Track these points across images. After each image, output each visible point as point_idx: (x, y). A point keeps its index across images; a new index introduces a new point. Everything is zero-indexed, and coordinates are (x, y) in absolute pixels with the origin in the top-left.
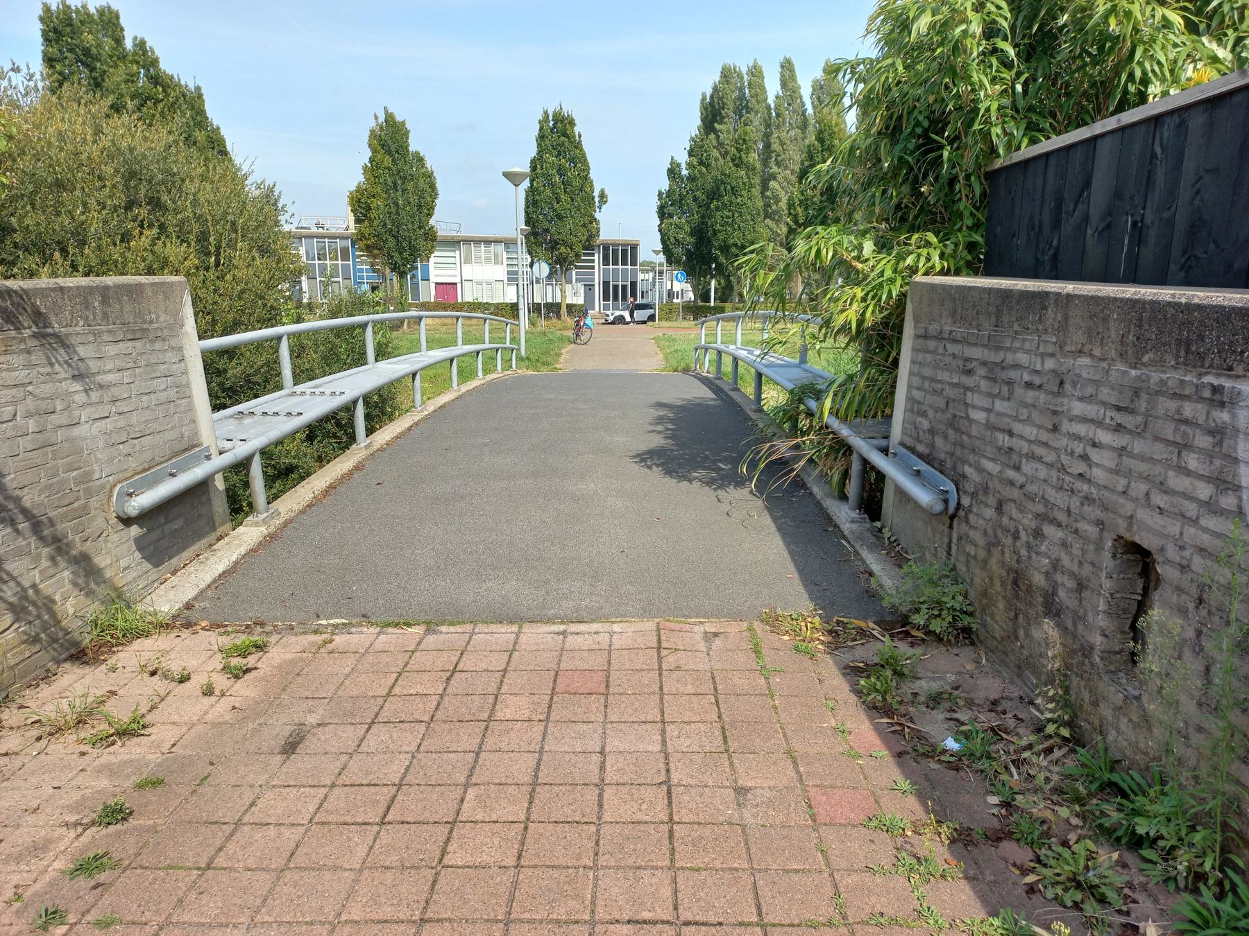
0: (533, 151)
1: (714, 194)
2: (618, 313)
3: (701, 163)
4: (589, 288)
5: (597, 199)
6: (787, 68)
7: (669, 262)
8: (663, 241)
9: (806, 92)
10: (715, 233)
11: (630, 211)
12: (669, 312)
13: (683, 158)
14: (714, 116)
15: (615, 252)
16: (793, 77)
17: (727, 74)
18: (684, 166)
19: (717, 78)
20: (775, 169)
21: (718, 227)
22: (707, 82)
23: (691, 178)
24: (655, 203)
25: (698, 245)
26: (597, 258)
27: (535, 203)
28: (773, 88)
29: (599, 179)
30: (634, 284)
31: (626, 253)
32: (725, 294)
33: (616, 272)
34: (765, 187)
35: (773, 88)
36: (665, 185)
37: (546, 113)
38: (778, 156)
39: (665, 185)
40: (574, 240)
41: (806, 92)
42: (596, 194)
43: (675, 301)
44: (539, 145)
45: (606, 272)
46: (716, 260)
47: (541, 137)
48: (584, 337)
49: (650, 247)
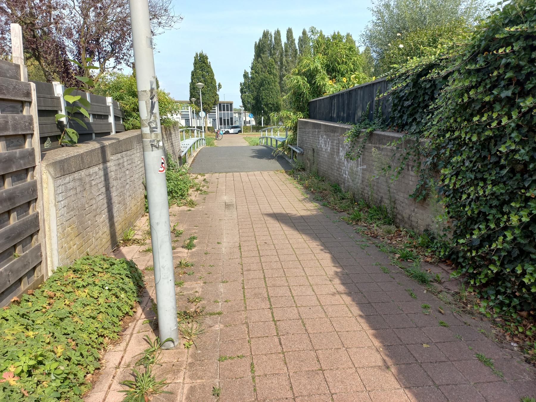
0: (192, 68)
1: (261, 85)
2: (226, 130)
3: (256, 72)
4: (214, 120)
5: (217, 87)
6: (290, 32)
7: (245, 110)
8: (243, 102)
9: (297, 42)
10: (263, 99)
11: (230, 91)
12: (247, 129)
13: (249, 70)
14: (260, 51)
15: (224, 106)
16: (292, 36)
17: (266, 35)
18: (249, 73)
19: (261, 36)
20: (285, 72)
21: (264, 97)
22: (257, 37)
23: (252, 78)
24: (239, 88)
25: (256, 104)
26: (217, 108)
27: (194, 88)
28: (284, 39)
29: (218, 79)
30: (232, 118)
31: (228, 106)
32: (267, 122)
33: (224, 114)
34: (281, 79)
35: (284, 39)
36: (242, 80)
37: (197, 54)
38: (286, 67)
39: (242, 80)
40: (209, 102)
41: (297, 42)
42: (217, 85)
43: (247, 125)
44: (195, 66)
45: (220, 114)
46: (263, 109)
47: (195, 64)
48: (220, 138)
49: (238, 104)
